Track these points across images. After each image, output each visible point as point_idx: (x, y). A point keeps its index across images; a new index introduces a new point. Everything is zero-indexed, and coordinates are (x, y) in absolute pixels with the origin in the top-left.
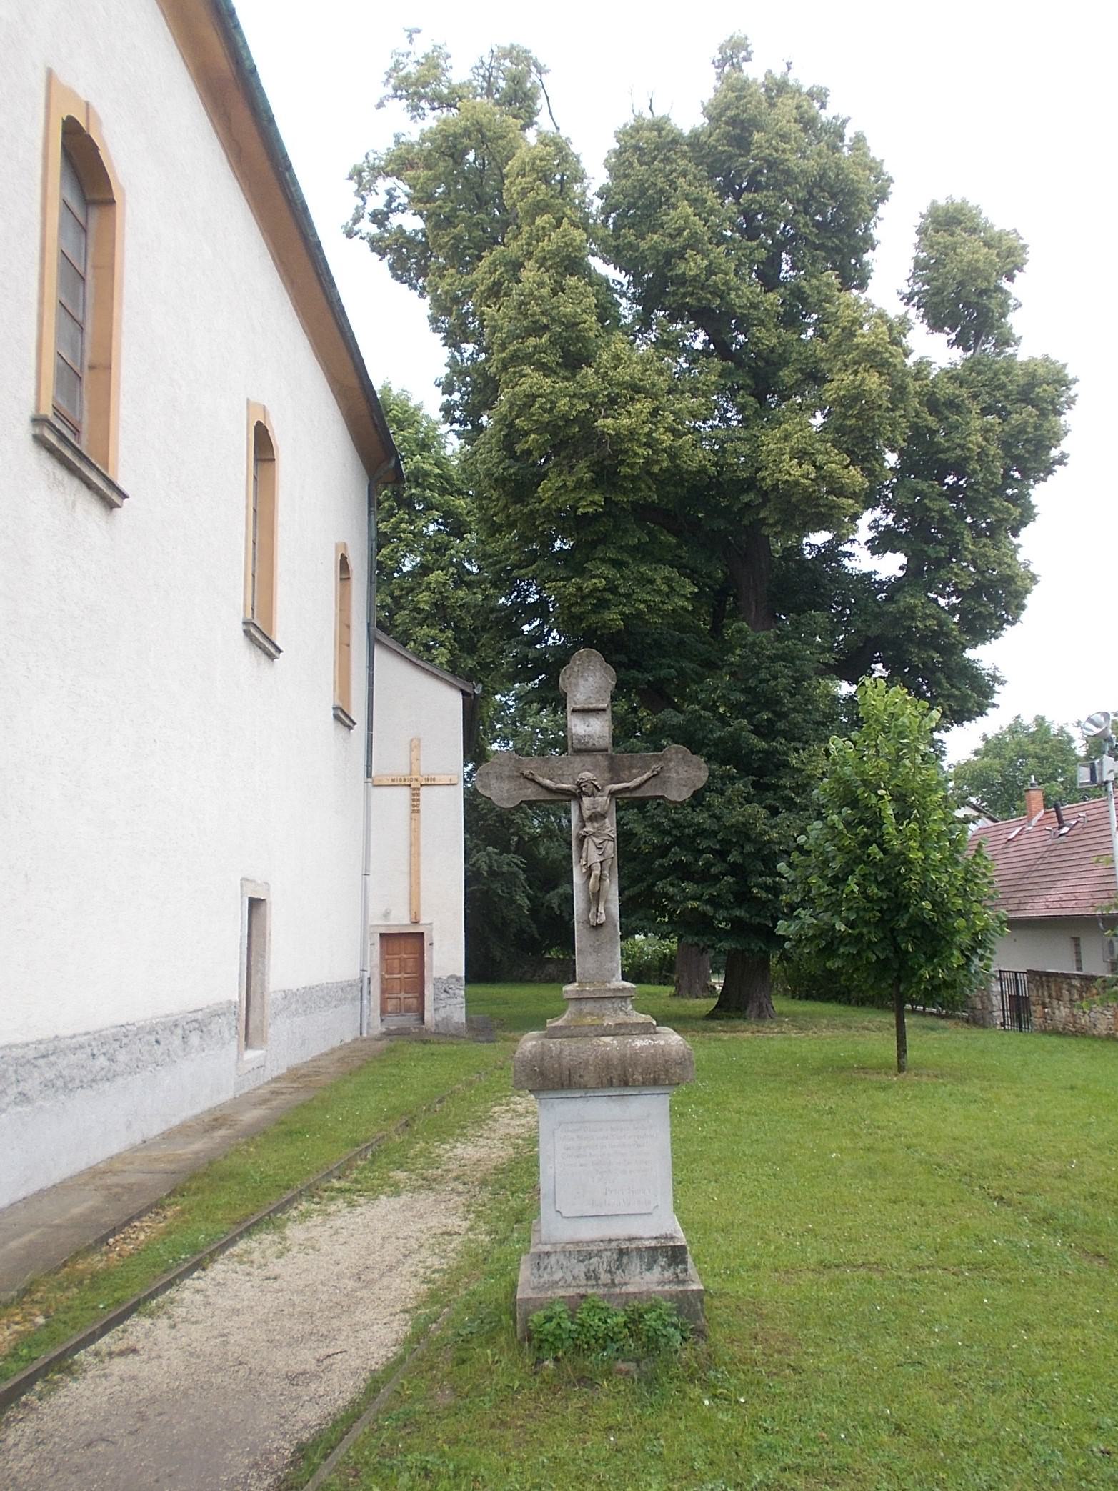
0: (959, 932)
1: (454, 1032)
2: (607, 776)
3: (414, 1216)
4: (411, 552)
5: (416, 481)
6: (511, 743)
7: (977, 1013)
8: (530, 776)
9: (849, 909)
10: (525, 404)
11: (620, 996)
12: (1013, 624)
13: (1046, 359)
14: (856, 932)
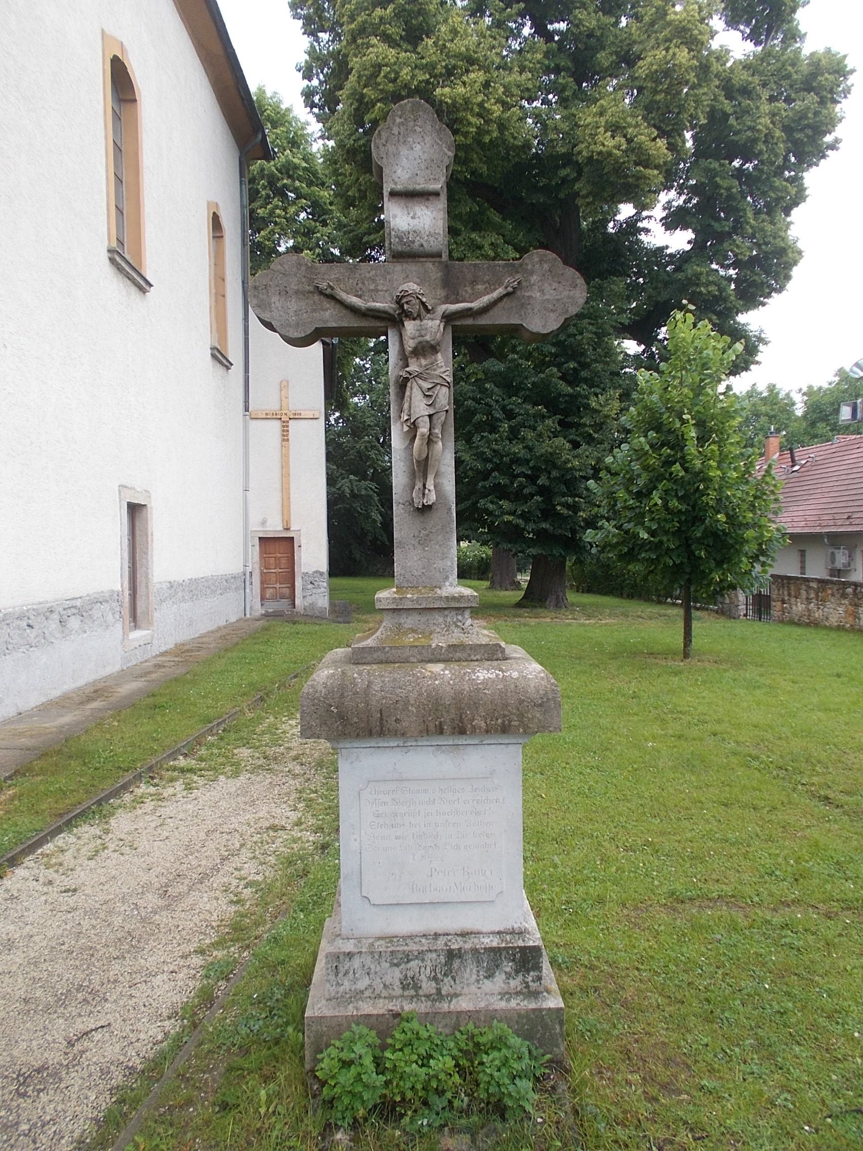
0: (747, 542)
1: (318, 614)
2: (441, 293)
3: (246, 803)
4: (285, 234)
5: (287, 173)
6: (368, 397)
7: (725, 606)
8: (329, 291)
9: (652, 520)
10: (372, 75)
11: (455, 607)
12: (780, 292)
13: (828, 51)
14: (656, 540)
